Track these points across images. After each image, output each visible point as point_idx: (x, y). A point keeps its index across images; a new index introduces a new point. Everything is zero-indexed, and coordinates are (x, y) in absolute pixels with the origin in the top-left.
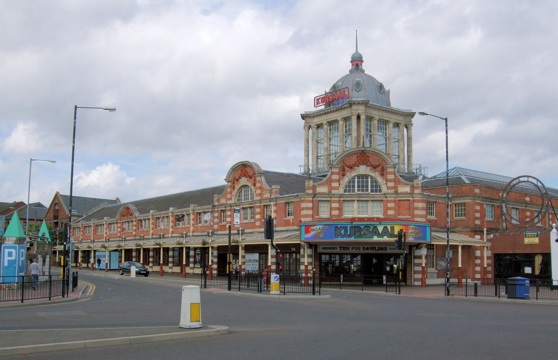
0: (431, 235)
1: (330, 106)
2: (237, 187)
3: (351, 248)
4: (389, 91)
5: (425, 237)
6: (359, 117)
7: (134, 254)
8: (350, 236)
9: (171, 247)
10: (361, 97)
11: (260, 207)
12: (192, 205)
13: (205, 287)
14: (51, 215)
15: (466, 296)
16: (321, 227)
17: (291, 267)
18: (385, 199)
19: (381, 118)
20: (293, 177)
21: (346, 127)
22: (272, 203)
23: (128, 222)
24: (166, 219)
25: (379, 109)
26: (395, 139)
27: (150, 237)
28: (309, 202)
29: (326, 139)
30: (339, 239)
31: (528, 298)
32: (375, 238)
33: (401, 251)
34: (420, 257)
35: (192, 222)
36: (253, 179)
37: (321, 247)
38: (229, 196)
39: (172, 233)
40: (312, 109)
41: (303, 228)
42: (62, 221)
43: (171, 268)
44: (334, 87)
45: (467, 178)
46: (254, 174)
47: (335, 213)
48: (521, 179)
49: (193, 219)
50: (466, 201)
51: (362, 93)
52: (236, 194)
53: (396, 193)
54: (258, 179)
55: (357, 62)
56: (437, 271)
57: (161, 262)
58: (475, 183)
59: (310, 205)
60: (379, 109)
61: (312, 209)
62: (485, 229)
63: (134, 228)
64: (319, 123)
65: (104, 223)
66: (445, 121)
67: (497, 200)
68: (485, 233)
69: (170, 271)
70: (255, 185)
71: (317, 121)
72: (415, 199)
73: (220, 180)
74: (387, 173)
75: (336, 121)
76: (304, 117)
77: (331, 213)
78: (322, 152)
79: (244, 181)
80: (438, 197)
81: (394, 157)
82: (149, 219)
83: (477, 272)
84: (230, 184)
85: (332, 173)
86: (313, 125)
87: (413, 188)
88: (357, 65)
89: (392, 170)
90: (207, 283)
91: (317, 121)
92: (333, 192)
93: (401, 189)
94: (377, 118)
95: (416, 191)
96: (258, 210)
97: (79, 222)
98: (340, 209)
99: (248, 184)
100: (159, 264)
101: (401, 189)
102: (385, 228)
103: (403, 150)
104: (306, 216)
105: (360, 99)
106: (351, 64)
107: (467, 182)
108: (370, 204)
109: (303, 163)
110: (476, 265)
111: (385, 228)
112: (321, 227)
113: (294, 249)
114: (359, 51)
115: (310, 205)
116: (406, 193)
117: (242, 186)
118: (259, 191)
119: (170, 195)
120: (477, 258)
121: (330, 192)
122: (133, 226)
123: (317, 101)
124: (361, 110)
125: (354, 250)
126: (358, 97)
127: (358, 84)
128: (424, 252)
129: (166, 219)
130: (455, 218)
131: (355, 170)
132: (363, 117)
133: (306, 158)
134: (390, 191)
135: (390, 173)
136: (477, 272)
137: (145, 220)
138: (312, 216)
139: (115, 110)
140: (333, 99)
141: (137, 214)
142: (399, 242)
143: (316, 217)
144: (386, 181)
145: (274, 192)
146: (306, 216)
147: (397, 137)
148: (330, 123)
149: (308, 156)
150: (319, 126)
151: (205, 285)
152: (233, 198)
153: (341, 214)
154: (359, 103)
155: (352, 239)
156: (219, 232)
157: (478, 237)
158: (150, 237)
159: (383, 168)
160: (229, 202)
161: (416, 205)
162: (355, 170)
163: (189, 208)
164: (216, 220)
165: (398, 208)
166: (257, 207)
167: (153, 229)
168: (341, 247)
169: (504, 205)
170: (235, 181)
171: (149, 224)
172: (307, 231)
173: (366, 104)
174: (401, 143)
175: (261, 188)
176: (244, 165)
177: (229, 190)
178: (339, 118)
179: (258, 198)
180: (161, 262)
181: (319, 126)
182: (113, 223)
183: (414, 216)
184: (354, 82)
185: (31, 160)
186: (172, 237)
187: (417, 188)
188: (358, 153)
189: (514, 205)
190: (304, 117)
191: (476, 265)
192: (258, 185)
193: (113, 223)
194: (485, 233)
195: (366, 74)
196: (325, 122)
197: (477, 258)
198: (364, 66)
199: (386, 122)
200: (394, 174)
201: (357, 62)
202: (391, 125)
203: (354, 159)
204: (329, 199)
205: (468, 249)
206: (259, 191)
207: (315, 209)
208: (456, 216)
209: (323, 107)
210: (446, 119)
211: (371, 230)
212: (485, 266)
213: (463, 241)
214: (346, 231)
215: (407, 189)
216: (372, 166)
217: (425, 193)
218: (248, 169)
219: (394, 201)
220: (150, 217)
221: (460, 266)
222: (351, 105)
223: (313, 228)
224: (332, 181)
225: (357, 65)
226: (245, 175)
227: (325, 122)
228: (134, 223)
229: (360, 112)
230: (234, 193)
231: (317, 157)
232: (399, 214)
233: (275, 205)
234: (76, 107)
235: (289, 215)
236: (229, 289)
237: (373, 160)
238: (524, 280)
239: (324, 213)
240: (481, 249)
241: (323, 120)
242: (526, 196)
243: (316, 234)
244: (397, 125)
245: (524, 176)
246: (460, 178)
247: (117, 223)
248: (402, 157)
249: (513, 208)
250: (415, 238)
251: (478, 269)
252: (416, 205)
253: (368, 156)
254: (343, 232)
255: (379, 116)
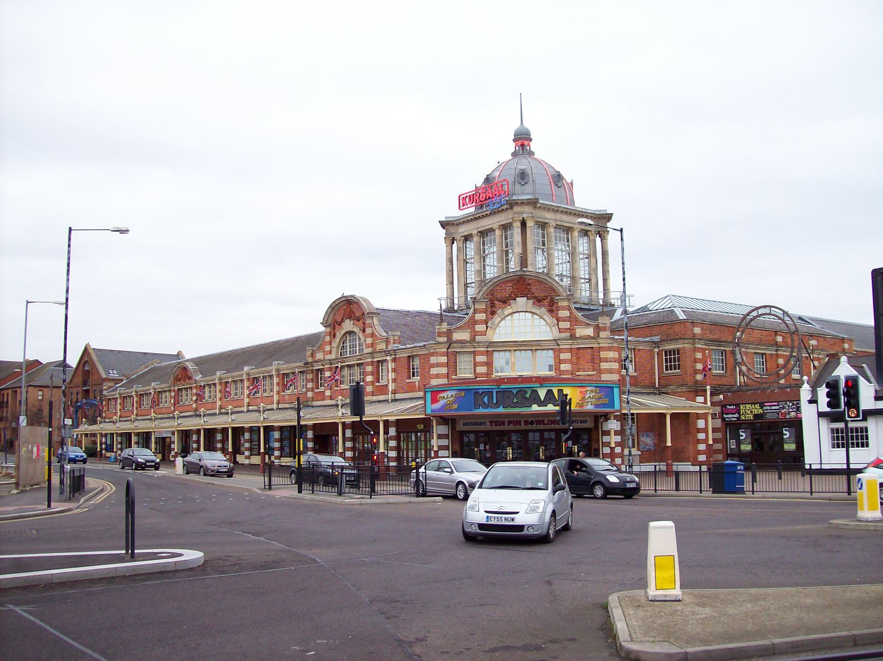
0: (620, 398)
1: (482, 207)
2: (339, 334)
3: (506, 423)
4: (572, 184)
5: (611, 404)
6: (523, 224)
7: (219, 437)
8: (497, 405)
9: (246, 426)
10: (529, 194)
11: (372, 363)
12: (276, 362)
13: (270, 488)
14: (79, 380)
15: (701, 491)
16: (454, 393)
17: (410, 454)
18: (557, 347)
19: (559, 223)
20: (425, 317)
21: (506, 239)
22: (388, 358)
23: (186, 389)
24: (239, 385)
25: (556, 210)
26: (584, 254)
27: (217, 411)
28: (442, 354)
29: (477, 257)
30: (481, 411)
31: (742, 491)
32: (535, 408)
33: (566, 426)
34: (607, 433)
35: (276, 389)
36: (361, 322)
37: (461, 422)
38: (328, 348)
39: (249, 405)
40: (454, 212)
41: (429, 395)
42: (95, 387)
43: (248, 458)
44: (488, 179)
45: (683, 311)
46: (363, 314)
47: (482, 370)
48: (761, 311)
49: (278, 384)
50: (680, 346)
51: (529, 188)
52: (338, 346)
53: (573, 337)
54: (368, 321)
55: (522, 139)
56: (639, 453)
57: (262, 450)
58: (693, 319)
59: (444, 359)
60: (556, 210)
61: (447, 365)
62: (708, 387)
63: (310, 385)
64: (466, 234)
65: (152, 391)
66: (619, 233)
67: (730, 342)
68: (708, 393)
69: (246, 462)
70: (364, 331)
71: (464, 230)
72: (601, 345)
73: (317, 327)
74: (558, 309)
75: (492, 230)
76: (444, 224)
77: (475, 371)
78: (472, 277)
79: (348, 325)
80: (638, 341)
81: (582, 281)
82: (242, 381)
83: (700, 452)
84: (328, 330)
85: (475, 311)
86: (458, 237)
87: (598, 329)
88: (523, 145)
89: (565, 304)
90: (273, 483)
91: (464, 230)
92: (478, 338)
93: (580, 332)
94: (553, 223)
95: (603, 334)
96: (369, 369)
97: (116, 389)
98: (489, 364)
99: (355, 330)
100: (259, 454)
101: (580, 332)
102: (550, 392)
103: (596, 270)
104: (437, 376)
105: (524, 197)
106: (514, 144)
107: (682, 316)
108: (539, 352)
109: (444, 294)
110: (699, 441)
111: (550, 392)
112: (454, 393)
113: (421, 427)
114: (526, 124)
115: (444, 359)
116: (589, 337)
117: (347, 333)
118: (369, 340)
119: (257, 346)
120: (699, 431)
121: (473, 339)
122: (307, 381)
123: (464, 201)
124: (526, 212)
125: (511, 425)
126: (523, 194)
127: (523, 175)
128: (613, 425)
129: (239, 385)
130: (665, 372)
131: (510, 305)
132: (530, 224)
133: (449, 286)
134: (563, 335)
135: (563, 308)
136: (700, 452)
137: (209, 385)
138: (448, 376)
139: (128, 231)
140: (488, 198)
141: (198, 377)
142: (563, 411)
143: (454, 377)
144: (558, 320)
145: (392, 342)
146: (437, 376)
147: (586, 252)
148: (483, 234)
149: (452, 283)
150: (467, 238)
151: (270, 485)
152: (334, 351)
153: (490, 373)
154: (523, 203)
155: (501, 410)
156: (315, 403)
157: (700, 399)
158: (245, 409)
159: (552, 300)
160: (328, 357)
161: (603, 354)
162: (510, 305)
163: (271, 368)
164: (369, 378)
165: (576, 363)
166: (368, 364)
167: (221, 399)
168: (491, 422)
169: (737, 349)
170: (337, 326)
171: (272, 384)
172: (434, 401)
173: (533, 203)
174: (593, 260)
175: (373, 335)
176: (348, 301)
177: (328, 339)
178: (495, 226)
179: (370, 350)
180: (262, 450)
181: (467, 238)
182: (165, 391)
183: (600, 372)
184: (517, 171)
185: (28, 302)
186: (248, 411)
187: (604, 329)
188: (513, 280)
189: (758, 349)
190: (444, 224)
191: (699, 441)
192: (368, 331)
193: (165, 391)
194: (708, 393)
195: (536, 159)
196: (553, 223)
197: (699, 431)
198: (534, 146)
199: (568, 230)
200: (569, 309)
201: (522, 139)
202: (576, 234)
203: (509, 288)
204: (473, 350)
205: (683, 420)
206: (369, 340)
207: (452, 366)
208: (667, 370)
209: (472, 210)
210: (621, 230)
211: (528, 396)
212: (711, 442)
213: (672, 408)
214: (491, 399)
215: (590, 331)
216: (535, 298)
217: (616, 337)
218: (354, 308)
219: (570, 350)
220: (217, 381)
221: (669, 444)
222: (512, 205)
223: (442, 395)
224: (475, 322)
225: (523, 145)
226: (350, 316)
227: (475, 232)
228: (194, 391)
229: (525, 216)
230: (335, 345)
231: (466, 285)
232: (579, 370)
233: (394, 360)
234: (70, 229)
235: (413, 376)
236: (300, 491)
237: (536, 290)
238: (735, 465)
239: (465, 371)
240: (704, 416)
241: (472, 228)
242: (776, 335)
243: (447, 404)
244: (585, 233)
245: (765, 307)
246: (673, 311)
247: (169, 391)
248: (593, 281)
249: (755, 353)
250: (597, 406)
251: (702, 447)
252: (603, 354)
253: (528, 284)
254: (486, 400)
255: (556, 220)
